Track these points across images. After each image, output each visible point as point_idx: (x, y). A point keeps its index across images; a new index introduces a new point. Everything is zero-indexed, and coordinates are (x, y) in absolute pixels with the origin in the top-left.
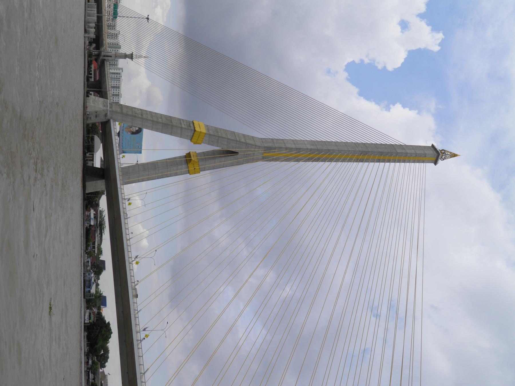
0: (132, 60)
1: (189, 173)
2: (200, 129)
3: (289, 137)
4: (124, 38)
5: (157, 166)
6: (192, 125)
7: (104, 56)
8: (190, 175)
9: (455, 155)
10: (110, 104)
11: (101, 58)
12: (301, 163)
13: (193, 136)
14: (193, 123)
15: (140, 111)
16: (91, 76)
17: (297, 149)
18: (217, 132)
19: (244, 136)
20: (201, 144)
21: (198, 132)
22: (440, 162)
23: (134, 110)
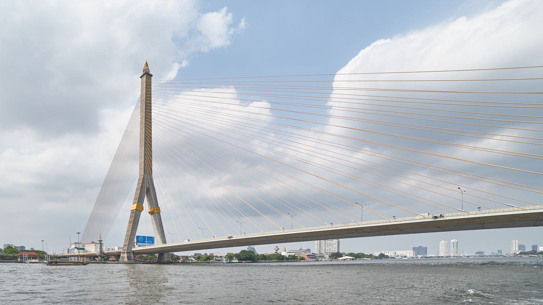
3: (138, 173)
6: (133, 211)
9: (147, 64)
12: (153, 154)
13: (139, 210)
14: (132, 210)
17: (145, 156)
18: (136, 198)
19: (138, 184)
21: (136, 208)
22: (151, 73)
23: (126, 240)
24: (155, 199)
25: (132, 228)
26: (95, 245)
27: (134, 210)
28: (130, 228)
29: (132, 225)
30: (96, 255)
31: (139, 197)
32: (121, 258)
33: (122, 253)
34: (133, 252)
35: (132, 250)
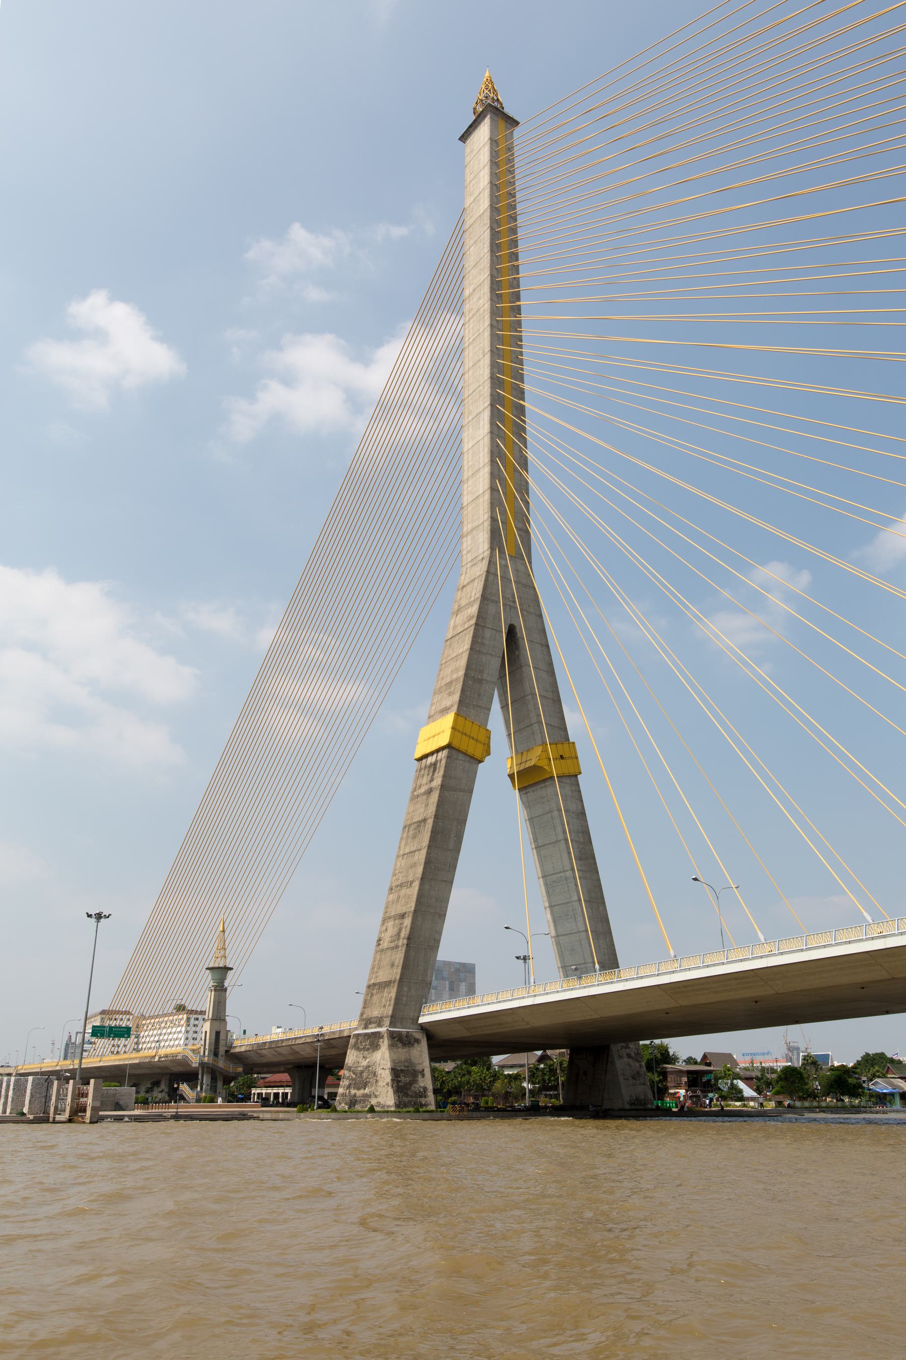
0: (232, 969)
1: (576, 776)
2: (443, 732)
4: (170, 1002)
5: (559, 875)
6: (431, 759)
7: (216, 1054)
8: (580, 773)
10: (366, 1027)
11: (221, 1063)
14: (426, 756)
15: (390, 924)
16: (264, 1094)
20: (489, 732)
21: (452, 736)
24: (550, 695)
25: (428, 862)
26: (188, 1019)
27: (438, 751)
28: (414, 865)
29: (429, 847)
30: (185, 1062)
31: (466, 675)
32: (344, 1083)
33: (356, 1047)
34: (428, 1031)
35: (422, 1020)
